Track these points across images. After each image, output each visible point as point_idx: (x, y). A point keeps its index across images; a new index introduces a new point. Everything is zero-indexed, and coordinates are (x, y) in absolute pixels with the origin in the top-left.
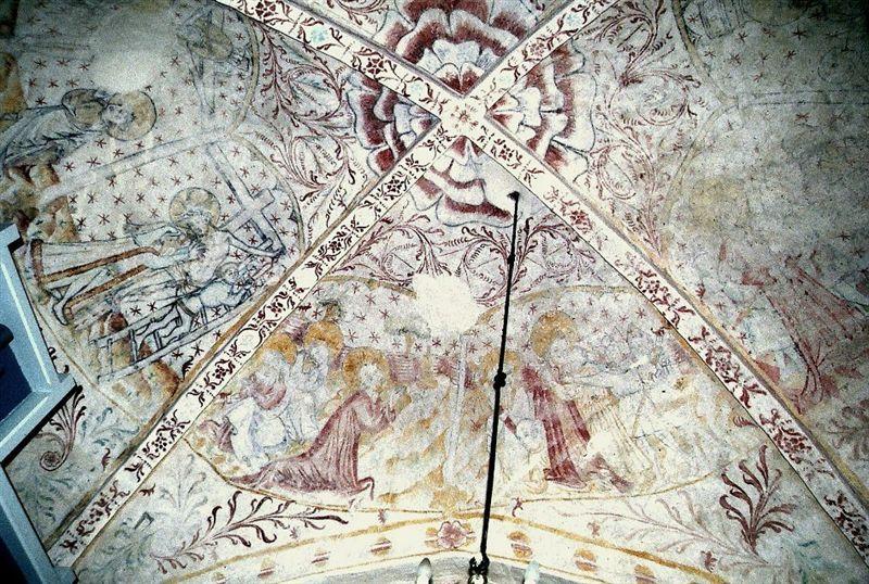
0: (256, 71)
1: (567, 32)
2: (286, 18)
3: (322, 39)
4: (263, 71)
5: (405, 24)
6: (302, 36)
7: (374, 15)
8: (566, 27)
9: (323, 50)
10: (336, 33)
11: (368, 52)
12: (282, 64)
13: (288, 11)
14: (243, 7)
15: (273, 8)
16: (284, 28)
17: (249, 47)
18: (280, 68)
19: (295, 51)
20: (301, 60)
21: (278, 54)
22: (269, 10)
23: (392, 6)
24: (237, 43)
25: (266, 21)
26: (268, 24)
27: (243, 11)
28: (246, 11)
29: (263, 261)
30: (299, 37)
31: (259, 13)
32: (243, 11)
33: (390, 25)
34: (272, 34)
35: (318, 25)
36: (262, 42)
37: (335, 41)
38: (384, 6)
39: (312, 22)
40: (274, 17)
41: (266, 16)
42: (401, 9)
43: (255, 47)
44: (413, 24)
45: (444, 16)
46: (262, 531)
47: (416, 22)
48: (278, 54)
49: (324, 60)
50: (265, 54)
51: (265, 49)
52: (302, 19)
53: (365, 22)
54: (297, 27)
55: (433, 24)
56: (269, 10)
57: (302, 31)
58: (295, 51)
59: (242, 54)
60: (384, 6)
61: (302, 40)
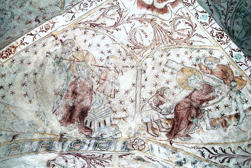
0: (239, 5)
1: (72, 12)
2: (213, 29)
3: (203, 16)
4: (236, 5)
5: (170, 6)
6: (210, 20)
7: (181, 14)
8: (71, 15)
9: (205, 11)
10: (197, 16)
11: (187, 4)
12: (226, 6)
13: (212, 31)
14: (228, 39)
15: (217, 35)
16: (216, 26)
17: (236, 17)
18: (227, 4)
19: (217, 11)
20: (217, 6)
21: (225, 12)
22: (219, 35)
23: (173, 15)
24: (240, 20)
25: (222, 31)
26: (222, 29)
27: (229, 38)
28: (228, 38)
29: (190, 88)
30: (212, 20)
31: (223, 35)
32: (229, 38)
33: (176, 8)
34: (224, 21)
35: (202, 22)
36: (230, 18)
37: (198, 13)
38: (176, 16)
39: (204, 24)
40: (218, 31)
41: (221, 33)
42: (170, 12)
43: (234, 17)
44: (167, 5)
45: (155, 4)
46: (209, 20)
47: (166, 6)
48: (225, 12)
49: (207, 4)
50: (231, 12)
51: (230, 15)
52: (207, 26)
53: (185, 13)
54: (211, 23)
55: (160, 2)
56: (219, 35)
57: (210, 22)
58: (217, 11)
59: (241, 15)
60: (176, 16)
61: (211, 18)
